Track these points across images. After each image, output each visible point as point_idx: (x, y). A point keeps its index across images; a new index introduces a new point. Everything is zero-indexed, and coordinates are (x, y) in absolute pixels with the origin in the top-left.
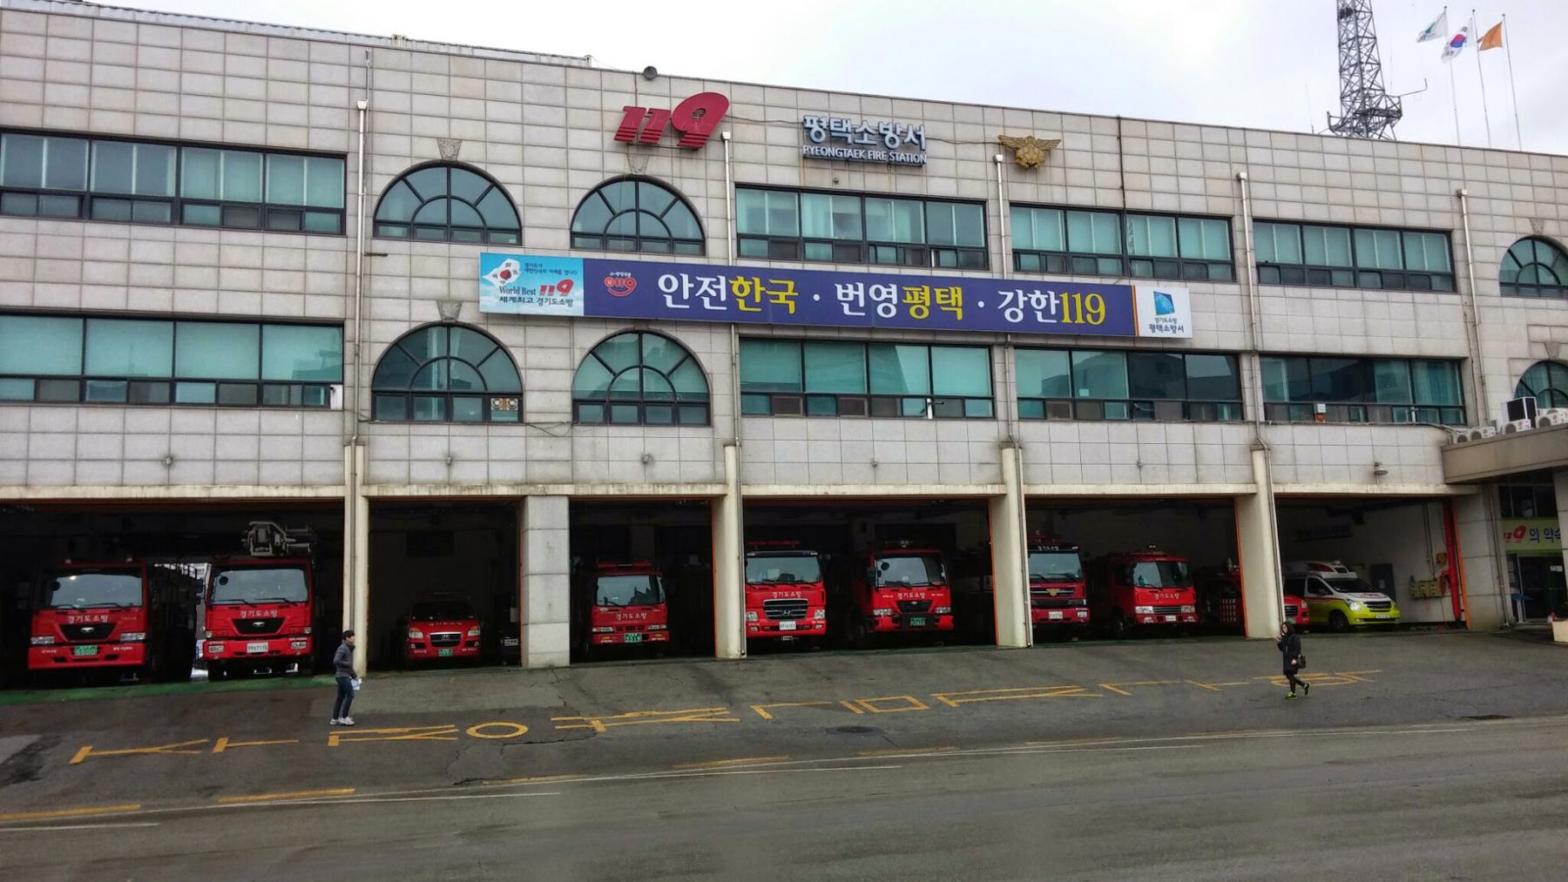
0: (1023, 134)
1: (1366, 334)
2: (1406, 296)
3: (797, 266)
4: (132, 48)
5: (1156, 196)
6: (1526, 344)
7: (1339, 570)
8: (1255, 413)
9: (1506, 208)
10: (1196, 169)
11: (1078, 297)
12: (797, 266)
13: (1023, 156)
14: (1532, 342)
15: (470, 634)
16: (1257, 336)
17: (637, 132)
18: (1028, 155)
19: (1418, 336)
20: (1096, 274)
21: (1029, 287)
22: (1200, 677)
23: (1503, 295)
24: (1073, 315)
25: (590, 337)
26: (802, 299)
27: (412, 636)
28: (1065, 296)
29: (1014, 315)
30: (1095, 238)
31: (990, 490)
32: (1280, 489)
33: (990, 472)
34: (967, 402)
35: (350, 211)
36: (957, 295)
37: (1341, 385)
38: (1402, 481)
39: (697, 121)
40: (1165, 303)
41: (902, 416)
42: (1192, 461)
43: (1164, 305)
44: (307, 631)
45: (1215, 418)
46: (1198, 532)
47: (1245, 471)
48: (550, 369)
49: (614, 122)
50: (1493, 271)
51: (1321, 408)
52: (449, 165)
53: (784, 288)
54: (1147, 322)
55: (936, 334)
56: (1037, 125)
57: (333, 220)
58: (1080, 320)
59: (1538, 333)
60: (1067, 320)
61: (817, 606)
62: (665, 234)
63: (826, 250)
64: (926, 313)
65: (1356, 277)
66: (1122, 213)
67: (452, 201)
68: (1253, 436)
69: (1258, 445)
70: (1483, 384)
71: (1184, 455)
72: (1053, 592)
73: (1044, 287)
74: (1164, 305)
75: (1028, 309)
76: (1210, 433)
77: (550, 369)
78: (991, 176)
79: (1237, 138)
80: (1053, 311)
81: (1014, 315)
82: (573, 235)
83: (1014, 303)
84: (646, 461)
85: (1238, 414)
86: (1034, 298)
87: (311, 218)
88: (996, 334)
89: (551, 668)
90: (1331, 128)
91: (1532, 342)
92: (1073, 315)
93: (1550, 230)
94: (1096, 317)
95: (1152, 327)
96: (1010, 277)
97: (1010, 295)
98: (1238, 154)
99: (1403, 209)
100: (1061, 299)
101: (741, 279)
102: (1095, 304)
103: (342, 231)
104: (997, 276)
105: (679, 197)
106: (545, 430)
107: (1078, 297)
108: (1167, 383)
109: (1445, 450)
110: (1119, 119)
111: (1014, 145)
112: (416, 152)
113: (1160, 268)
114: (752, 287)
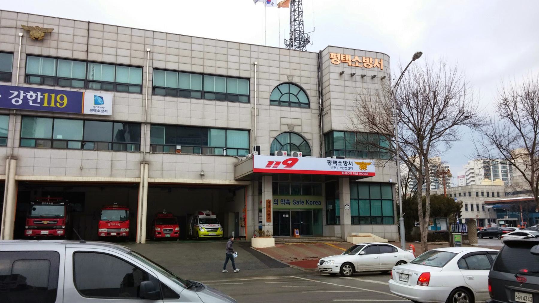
0: (34, 25)
1: (203, 118)
2: (225, 103)
3: (68, 89)
4: (249, 52)
5: (104, 56)
6: (279, 125)
7: (207, 215)
8: (145, 148)
9: (276, 70)
11: (53, 96)
12: (68, 89)
14: (282, 124)
15: (176, 229)
18: (38, 34)
19: (228, 119)
20: (71, 87)
21: (26, 90)
23: (270, 105)
27: (157, 230)
28: (46, 95)
29: (17, 101)
30: (76, 72)
31: (137, 180)
32: (152, 180)
33: (137, 173)
34: (69, 142)
35: (252, 95)
37: (191, 138)
38: (214, 178)
40: (99, 100)
41: (214, 155)
42: (110, 168)
43: (98, 101)
44: (63, 227)
50: (267, 95)
51: (179, 147)
52: (289, 83)
55: (53, 114)
56: (45, 22)
57: (138, 89)
58: (53, 105)
59: (284, 121)
60: (46, 104)
62: (297, 101)
63: (38, 79)
64: (21, 102)
65: (203, 95)
68: (142, 158)
69: (144, 162)
70: (255, 140)
72: (45, 223)
73: (35, 90)
74: (98, 101)
75: (25, 99)
76: (121, 156)
78: (253, 69)
79: (149, 34)
80: (39, 101)
81: (17, 101)
82: (271, 101)
85: (138, 149)
86: (29, 95)
87: (193, 94)
88: (9, 110)
90: (286, 45)
91: (282, 124)
93: (296, 80)
94: (61, 104)
95: (91, 110)
96: (21, 85)
97: (16, 93)
98: (150, 41)
99: (227, 68)
100: (44, 96)
101: (31, 93)
102: (62, 99)
103: (141, 92)
104: (13, 85)
105: (301, 89)
107: (53, 96)
109: (236, 166)
110: (89, 22)
111: (28, 29)
112: (281, 79)
113: (105, 86)
114: (37, 96)
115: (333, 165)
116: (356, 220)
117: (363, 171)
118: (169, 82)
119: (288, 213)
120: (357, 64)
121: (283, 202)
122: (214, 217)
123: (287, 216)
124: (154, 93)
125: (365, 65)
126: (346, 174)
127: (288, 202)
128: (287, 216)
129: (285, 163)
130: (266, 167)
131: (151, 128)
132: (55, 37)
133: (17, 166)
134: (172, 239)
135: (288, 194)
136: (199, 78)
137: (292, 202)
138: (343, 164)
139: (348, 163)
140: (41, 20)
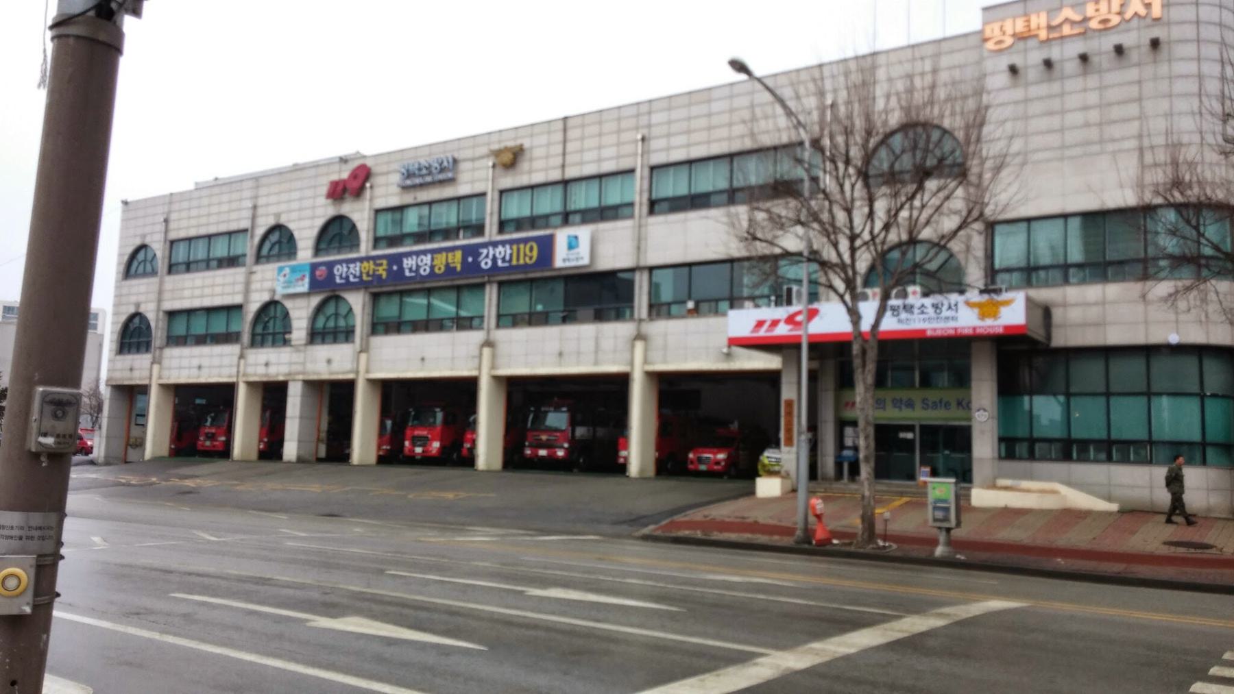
10: (613, 139)
13: (511, 158)
16: (642, 257)
17: (338, 192)
22: (443, 488)
24: (518, 259)
25: (315, 300)
26: (389, 271)
30: (549, 203)
32: (651, 368)
36: (459, 254)
39: (354, 183)
44: (566, 445)
45: (138, 351)
46: (600, 397)
47: (627, 355)
48: (300, 316)
49: (324, 190)
53: (381, 265)
54: (562, 258)
61: (433, 439)
66: (565, 183)
67: (279, 241)
69: (640, 336)
71: (588, 346)
73: (503, 243)
74: (572, 244)
75: (494, 259)
77: (300, 316)
79: (794, 76)
83: (487, 256)
84: (329, 361)
89: (289, 462)
92: (518, 259)
94: (531, 258)
102: (531, 249)
106: (297, 349)
107: (522, 246)
108: (600, 294)
115: (904, 315)
116: (1022, 449)
117: (989, 322)
118: (675, 186)
119: (910, 428)
120: (1066, 30)
121: (897, 403)
122: (902, 435)
123: (910, 436)
124: (652, 211)
125: (1094, 24)
126: (939, 333)
127: (947, 405)
128: (910, 436)
129: (790, 320)
130: (753, 331)
131: (566, 285)
132: (527, 155)
133: (646, 350)
134: (711, 475)
135: (912, 386)
136: (684, 172)
137: (918, 405)
138: (930, 310)
139: (945, 307)
140: (512, 134)
